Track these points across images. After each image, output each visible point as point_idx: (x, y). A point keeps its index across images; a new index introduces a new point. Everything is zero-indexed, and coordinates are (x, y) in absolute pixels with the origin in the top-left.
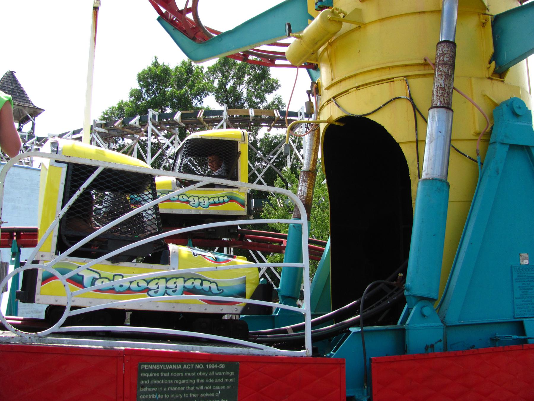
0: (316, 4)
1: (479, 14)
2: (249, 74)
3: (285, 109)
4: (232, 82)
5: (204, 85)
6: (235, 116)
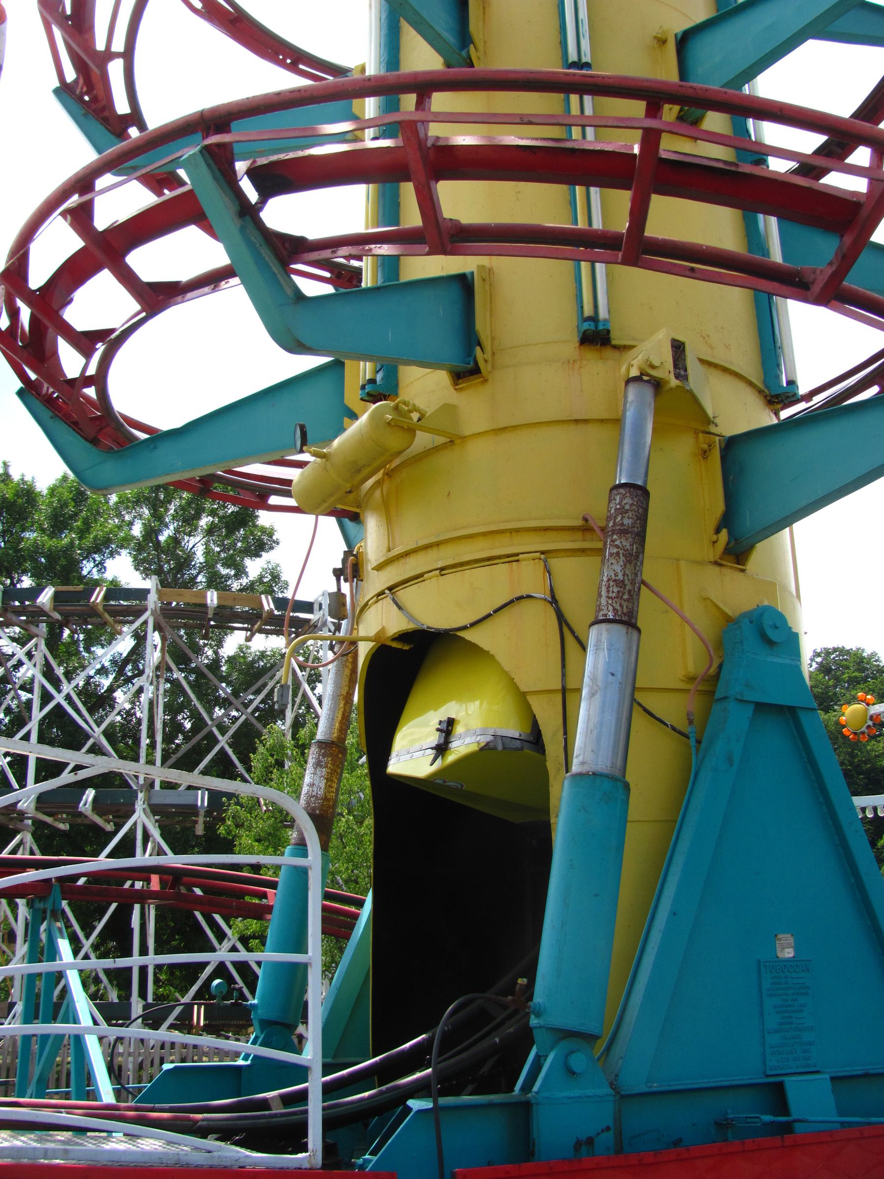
0: (363, 387)
1: (696, 432)
2: (213, 513)
3: (288, 594)
4: (172, 527)
5: (111, 532)
6: (174, 604)
